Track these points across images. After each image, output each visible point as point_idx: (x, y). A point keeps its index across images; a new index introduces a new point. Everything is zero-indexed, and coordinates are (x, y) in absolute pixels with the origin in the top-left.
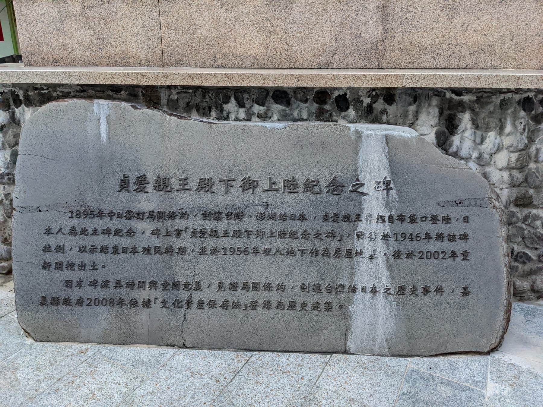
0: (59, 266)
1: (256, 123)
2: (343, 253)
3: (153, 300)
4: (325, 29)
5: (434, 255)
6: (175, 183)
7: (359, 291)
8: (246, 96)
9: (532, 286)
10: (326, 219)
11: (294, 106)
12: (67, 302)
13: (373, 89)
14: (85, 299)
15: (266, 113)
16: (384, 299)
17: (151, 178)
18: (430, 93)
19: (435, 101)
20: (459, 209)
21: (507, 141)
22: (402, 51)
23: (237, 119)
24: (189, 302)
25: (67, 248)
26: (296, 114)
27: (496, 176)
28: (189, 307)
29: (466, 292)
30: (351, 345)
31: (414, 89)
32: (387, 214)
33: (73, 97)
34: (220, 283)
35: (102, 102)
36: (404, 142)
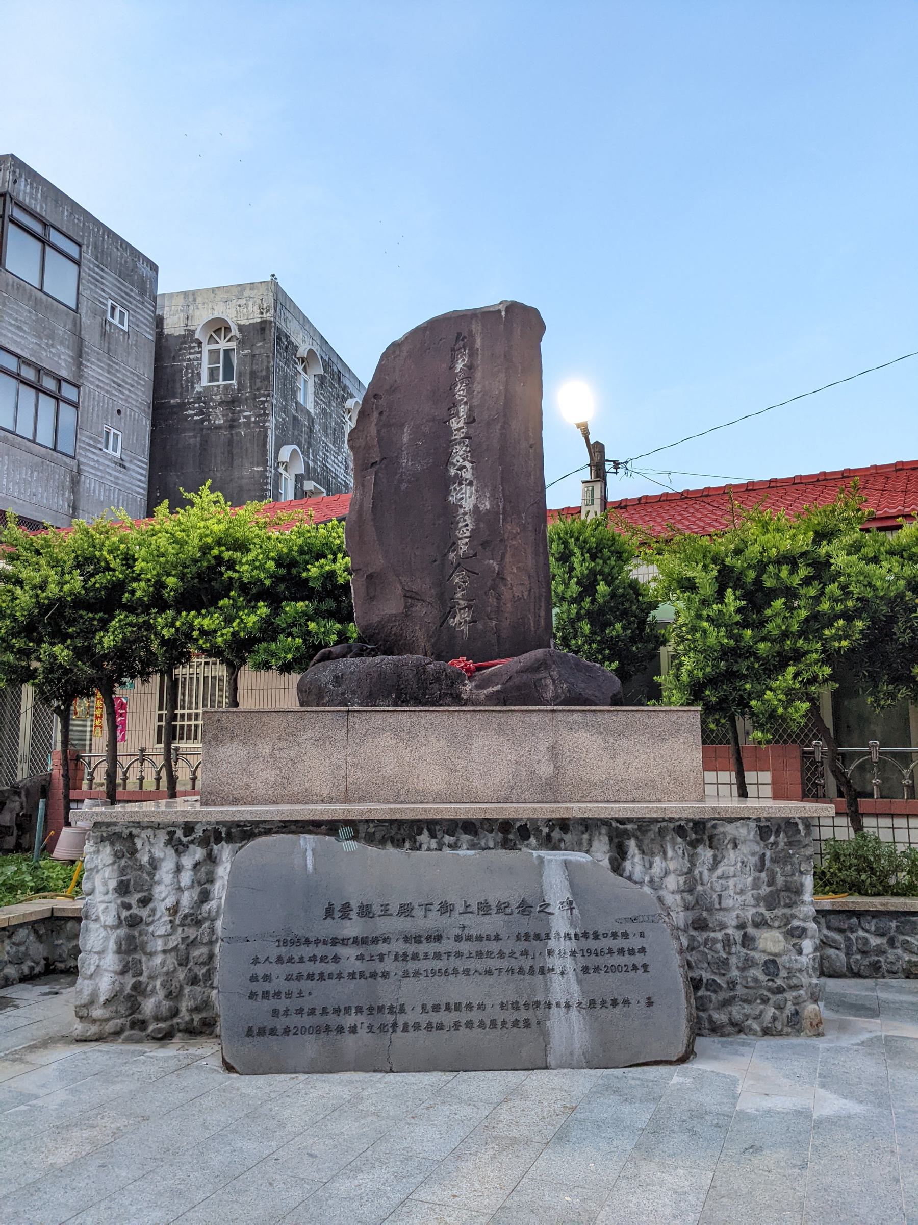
0: (266, 995)
1: (447, 851)
2: (537, 970)
3: (359, 1026)
4: (502, 767)
5: (616, 969)
6: (376, 909)
7: (554, 1006)
8: (438, 828)
9: (730, 1019)
10: (518, 938)
11: (482, 836)
12: (273, 1032)
13: (550, 820)
14: (292, 1028)
15: (455, 843)
16: (577, 1013)
17: (355, 905)
18: (599, 823)
19: (604, 830)
20: (635, 924)
21: (672, 865)
22: (574, 786)
23: (429, 849)
24: (395, 1025)
25: (274, 977)
26: (483, 843)
27: (670, 899)
28: (394, 1031)
29: (650, 1003)
30: (551, 1060)
31: (584, 819)
32: (572, 932)
33: (276, 833)
34: (423, 1005)
35: (307, 836)
36: (580, 865)
